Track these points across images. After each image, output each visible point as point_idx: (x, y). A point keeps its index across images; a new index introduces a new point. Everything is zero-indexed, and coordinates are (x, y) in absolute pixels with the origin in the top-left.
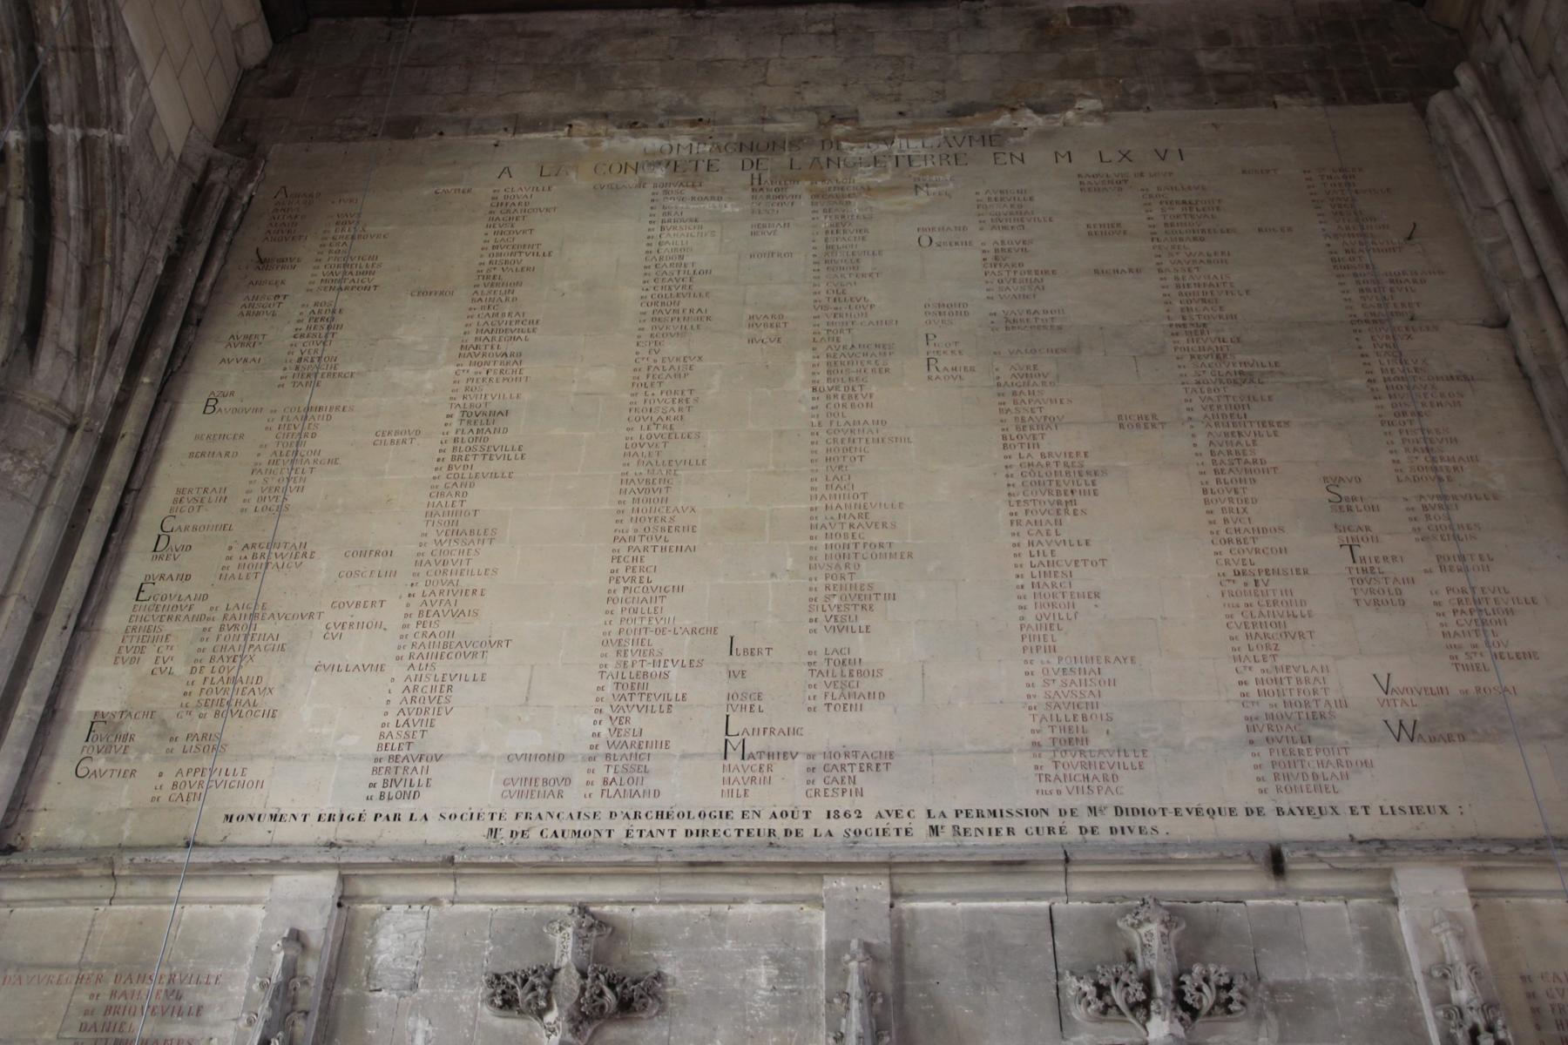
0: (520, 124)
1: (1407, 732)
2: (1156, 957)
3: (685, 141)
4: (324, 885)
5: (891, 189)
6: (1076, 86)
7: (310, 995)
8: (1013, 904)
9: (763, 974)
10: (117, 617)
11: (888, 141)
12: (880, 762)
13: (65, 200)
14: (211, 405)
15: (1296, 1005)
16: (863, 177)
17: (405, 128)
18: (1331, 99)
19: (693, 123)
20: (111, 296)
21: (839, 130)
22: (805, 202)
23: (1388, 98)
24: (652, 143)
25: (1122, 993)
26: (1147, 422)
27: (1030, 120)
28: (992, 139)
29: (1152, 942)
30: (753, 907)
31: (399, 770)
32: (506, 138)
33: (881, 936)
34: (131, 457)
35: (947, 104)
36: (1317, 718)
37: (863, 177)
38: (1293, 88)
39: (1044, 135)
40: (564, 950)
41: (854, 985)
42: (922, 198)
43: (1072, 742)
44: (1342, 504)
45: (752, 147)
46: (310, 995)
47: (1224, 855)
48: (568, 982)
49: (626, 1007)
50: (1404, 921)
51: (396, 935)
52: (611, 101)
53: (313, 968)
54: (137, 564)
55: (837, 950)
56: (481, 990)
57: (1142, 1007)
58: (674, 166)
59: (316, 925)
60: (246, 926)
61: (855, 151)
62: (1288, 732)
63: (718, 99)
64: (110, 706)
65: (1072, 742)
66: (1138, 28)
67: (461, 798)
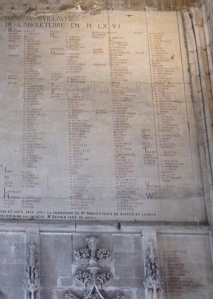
1: (150, 196)
2: (93, 248)
9: (13, 248)
12: (38, 200)
18: (160, 9)
23: (175, 9)
33: (37, 241)
36: (132, 192)
43: (78, 196)
50: (144, 239)
55: (29, 244)
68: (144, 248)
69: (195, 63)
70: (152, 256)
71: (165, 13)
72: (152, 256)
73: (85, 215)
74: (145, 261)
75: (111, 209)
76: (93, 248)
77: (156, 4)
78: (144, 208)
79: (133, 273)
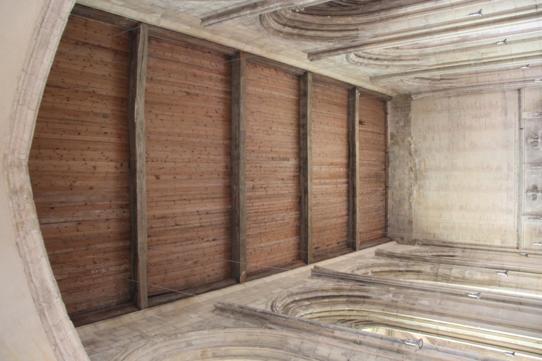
0: (410, 208)
1: (506, 114)
2: (533, 140)
3: (415, 188)
4: (523, 218)
5: (425, 163)
6: (406, 140)
7: (535, 217)
8: (526, 153)
9: (533, 176)
10: (488, 243)
11: (416, 164)
12: (509, 165)
13: (498, 289)
14: (457, 239)
15: (536, 128)
16: (423, 166)
17: (410, 222)
18: (410, 110)
19: (411, 186)
20: (255, 206)
21: (413, 169)
22: (427, 173)
23: (410, 103)
24: (415, 192)
25: (535, 144)
26: (464, 136)
27: (413, 146)
28: (416, 151)
29: (530, 140)
30: (525, 177)
31: (509, 212)
32: (413, 210)
33: (530, 165)
34: (250, 206)
35: (409, 156)
36: (504, 123)
37: (423, 166)
38: (408, 114)
39: (415, 145)
40: (530, 194)
41: (535, 167)
42: (427, 160)
43: (507, 147)
44: (476, 117)
45: (416, 179)
46: (535, 217)
47: (520, 134)
48: (534, 193)
49: (536, 188)
50: (527, 117)
51: (529, 210)
52: (407, 197)
53: (532, 217)
54: (482, 243)
55: (531, 169)
56: (534, 201)
57: (537, 142)
58: (419, 189)
59: (527, 217)
60: (527, 223)
61: (418, 167)
62: (506, 126)
63: (407, 184)
64: (500, 242)
65: (507, 147)
66: (395, 132)
67: (513, 205)
68: (532, 117)
69: (478, 82)
70: (536, 114)
71: (412, 108)
72: (536, 114)
73: (516, 144)
74: (538, 117)
75: (513, 133)
76: (533, 140)
77: (358, 94)
78: (513, 117)
79: (144, 83)
